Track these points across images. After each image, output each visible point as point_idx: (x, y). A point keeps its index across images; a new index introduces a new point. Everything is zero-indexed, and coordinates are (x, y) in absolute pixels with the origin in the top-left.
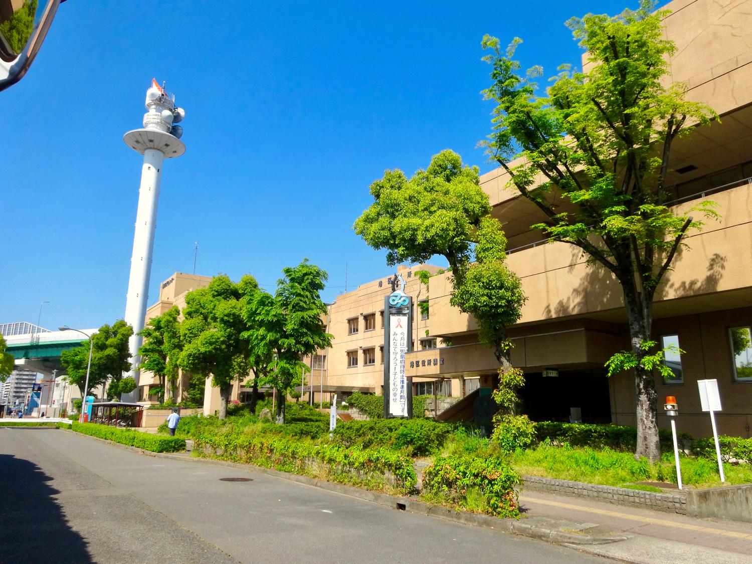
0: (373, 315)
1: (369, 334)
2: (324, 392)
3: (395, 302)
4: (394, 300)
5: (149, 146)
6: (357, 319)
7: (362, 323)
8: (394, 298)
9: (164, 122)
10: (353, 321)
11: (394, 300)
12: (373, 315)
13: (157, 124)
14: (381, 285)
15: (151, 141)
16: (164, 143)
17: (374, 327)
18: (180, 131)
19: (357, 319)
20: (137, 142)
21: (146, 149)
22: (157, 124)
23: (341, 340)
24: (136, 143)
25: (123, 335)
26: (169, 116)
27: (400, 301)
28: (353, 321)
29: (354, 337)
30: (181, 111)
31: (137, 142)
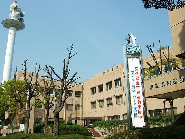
0: (102, 85)
1: (101, 93)
2: (82, 120)
3: (130, 50)
4: (129, 49)
5: (11, 25)
6: (95, 88)
7: (97, 89)
8: (130, 47)
9: (17, 16)
10: (93, 89)
11: (129, 49)
12: (102, 85)
13: (14, 17)
14: (104, 73)
15: (12, 23)
16: (17, 24)
17: (103, 91)
18: (23, 20)
19: (95, 88)
20: (7, 24)
21: (10, 27)
22: (14, 17)
23: (87, 98)
24: (6, 25)
25: (69, 118)
26: (18, 14)
27: (133, 49)
28: (93, 89)
29: (94, 95)
30: (16, 1)
31: (7, 24)
